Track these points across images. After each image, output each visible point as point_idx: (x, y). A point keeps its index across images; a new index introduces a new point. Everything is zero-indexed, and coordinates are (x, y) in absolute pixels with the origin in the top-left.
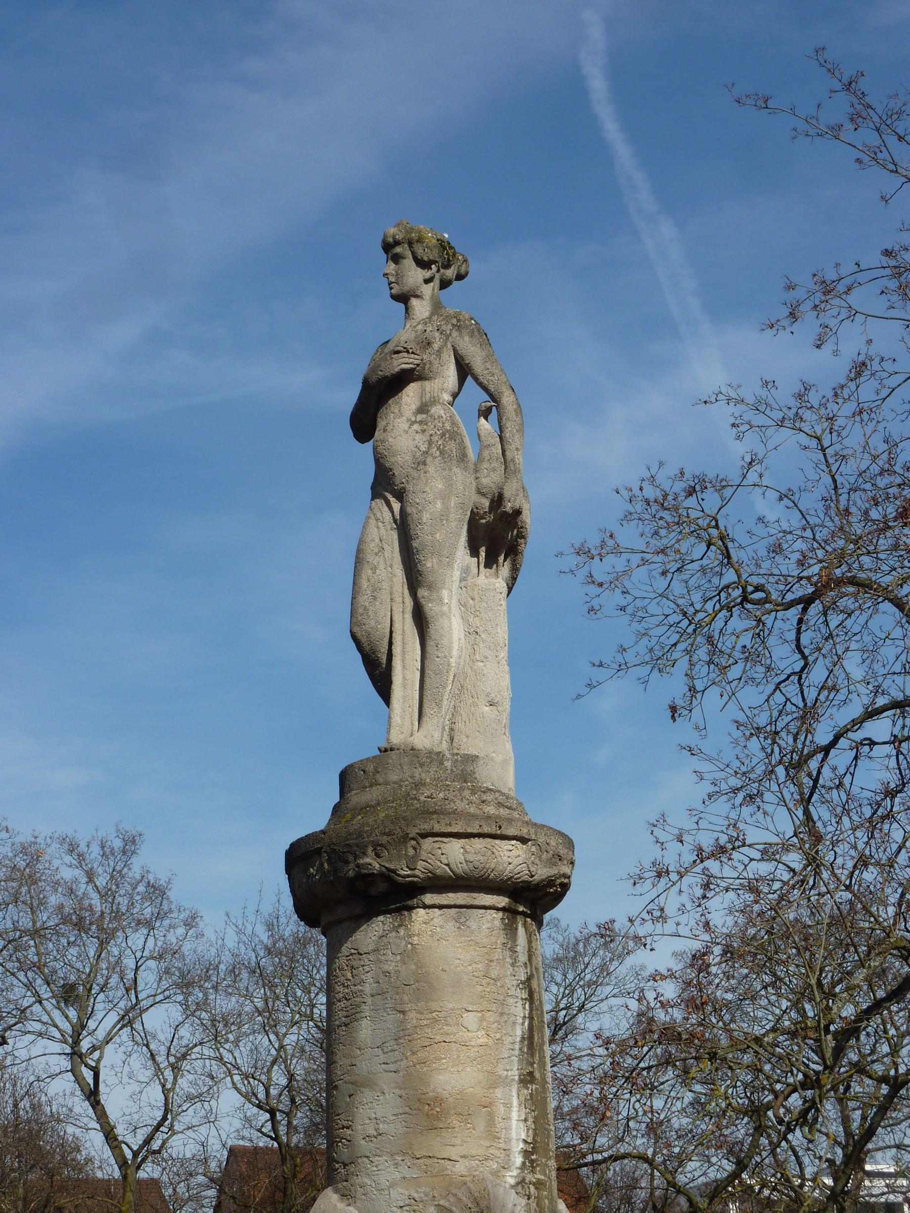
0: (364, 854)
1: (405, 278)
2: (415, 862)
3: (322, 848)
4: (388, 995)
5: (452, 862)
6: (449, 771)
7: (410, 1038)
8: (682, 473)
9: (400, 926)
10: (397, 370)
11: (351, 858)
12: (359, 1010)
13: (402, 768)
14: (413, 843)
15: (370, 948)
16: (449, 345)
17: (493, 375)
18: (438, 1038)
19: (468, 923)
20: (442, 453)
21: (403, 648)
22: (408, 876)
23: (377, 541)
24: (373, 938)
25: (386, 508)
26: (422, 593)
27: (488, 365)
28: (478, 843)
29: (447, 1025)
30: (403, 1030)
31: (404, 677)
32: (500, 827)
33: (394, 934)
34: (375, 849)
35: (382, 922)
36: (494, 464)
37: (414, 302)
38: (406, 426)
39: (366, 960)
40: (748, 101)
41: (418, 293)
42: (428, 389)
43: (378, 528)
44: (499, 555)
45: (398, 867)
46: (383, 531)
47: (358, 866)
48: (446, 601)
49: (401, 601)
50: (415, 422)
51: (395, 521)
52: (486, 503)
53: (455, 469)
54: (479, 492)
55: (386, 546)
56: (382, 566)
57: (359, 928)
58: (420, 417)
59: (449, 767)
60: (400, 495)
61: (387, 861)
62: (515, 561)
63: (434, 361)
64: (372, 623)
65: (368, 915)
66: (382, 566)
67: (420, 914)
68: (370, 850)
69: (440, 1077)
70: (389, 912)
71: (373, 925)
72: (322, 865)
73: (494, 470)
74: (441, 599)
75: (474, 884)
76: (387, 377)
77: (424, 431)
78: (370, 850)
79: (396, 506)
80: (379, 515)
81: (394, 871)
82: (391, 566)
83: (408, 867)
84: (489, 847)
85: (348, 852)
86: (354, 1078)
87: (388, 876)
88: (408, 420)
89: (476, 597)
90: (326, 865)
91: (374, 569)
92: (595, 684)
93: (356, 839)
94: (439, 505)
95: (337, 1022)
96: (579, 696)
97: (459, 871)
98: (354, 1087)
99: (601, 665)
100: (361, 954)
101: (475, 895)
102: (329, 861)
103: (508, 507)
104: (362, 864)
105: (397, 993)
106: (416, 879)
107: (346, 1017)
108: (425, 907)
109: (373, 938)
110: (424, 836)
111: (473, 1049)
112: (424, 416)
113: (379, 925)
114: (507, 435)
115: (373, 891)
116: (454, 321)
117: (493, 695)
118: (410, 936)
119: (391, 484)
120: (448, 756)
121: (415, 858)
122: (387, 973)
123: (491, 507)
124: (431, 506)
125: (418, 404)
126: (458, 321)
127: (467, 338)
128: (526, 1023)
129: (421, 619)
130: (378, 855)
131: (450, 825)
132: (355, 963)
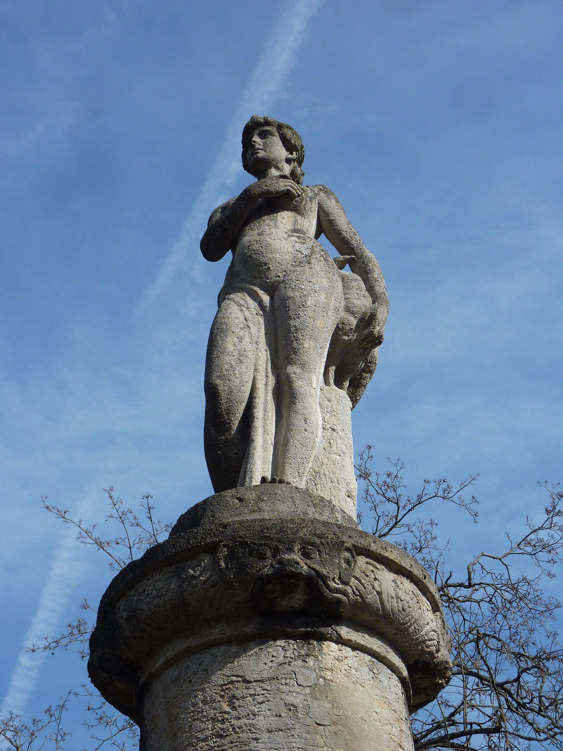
0: (290, 550)
3: (221, 541)
5: (384, 591)
9: (308, 655)
11: (269, 554)
13: (294, 501)
14: (347, 555)
16: (317, 202)
19: (380, 677)
21: (265, 415)
22: (338, 591)
23: (242, 319)
28: (409, 586)
31: (264, 441)
33: (300, 662)
35: (283, 648)
38: (286, 236)
39: (258, 689)
40: (53, 510)
42: (299, 221)
45: (331, 575)
46: (247, 314)
47: (281, 562)
48: (314, 386)
49: (264, 374)
50: (293, 236)
52: (353, 321)
54: (348, 310)
55: (251, 325)
56: (247, 339)
60: (272, 289)
61: (319, 564)
63: (308, 202)
64: (237, 382)
65: (263, 637)
66: (247, 339)
67: (331, 648)
68: (297, 547)
70: (294, 637)
71: (270, 650)
72: (216, 562)
78: (297, 547)
79: (266, 299)
80: (242, 302)
81: (324, 579)
83: (340, 578)
85: (266, 545)
87: (314, 583)
90: (222, 564)
91: (241, 339)
93: (276, 533)
101: (389, 649)
102: (231, 557)
104: (288, 560)
105: (308, 732)
106: (344, 598)
108: (340, 641)
113: (280, 650)
114: (376, 276)
115: (284, 604)
119: (261, 278)
122: (292, 708)
123: (358, 326)
130: (306, 555)
132: (238, 693)
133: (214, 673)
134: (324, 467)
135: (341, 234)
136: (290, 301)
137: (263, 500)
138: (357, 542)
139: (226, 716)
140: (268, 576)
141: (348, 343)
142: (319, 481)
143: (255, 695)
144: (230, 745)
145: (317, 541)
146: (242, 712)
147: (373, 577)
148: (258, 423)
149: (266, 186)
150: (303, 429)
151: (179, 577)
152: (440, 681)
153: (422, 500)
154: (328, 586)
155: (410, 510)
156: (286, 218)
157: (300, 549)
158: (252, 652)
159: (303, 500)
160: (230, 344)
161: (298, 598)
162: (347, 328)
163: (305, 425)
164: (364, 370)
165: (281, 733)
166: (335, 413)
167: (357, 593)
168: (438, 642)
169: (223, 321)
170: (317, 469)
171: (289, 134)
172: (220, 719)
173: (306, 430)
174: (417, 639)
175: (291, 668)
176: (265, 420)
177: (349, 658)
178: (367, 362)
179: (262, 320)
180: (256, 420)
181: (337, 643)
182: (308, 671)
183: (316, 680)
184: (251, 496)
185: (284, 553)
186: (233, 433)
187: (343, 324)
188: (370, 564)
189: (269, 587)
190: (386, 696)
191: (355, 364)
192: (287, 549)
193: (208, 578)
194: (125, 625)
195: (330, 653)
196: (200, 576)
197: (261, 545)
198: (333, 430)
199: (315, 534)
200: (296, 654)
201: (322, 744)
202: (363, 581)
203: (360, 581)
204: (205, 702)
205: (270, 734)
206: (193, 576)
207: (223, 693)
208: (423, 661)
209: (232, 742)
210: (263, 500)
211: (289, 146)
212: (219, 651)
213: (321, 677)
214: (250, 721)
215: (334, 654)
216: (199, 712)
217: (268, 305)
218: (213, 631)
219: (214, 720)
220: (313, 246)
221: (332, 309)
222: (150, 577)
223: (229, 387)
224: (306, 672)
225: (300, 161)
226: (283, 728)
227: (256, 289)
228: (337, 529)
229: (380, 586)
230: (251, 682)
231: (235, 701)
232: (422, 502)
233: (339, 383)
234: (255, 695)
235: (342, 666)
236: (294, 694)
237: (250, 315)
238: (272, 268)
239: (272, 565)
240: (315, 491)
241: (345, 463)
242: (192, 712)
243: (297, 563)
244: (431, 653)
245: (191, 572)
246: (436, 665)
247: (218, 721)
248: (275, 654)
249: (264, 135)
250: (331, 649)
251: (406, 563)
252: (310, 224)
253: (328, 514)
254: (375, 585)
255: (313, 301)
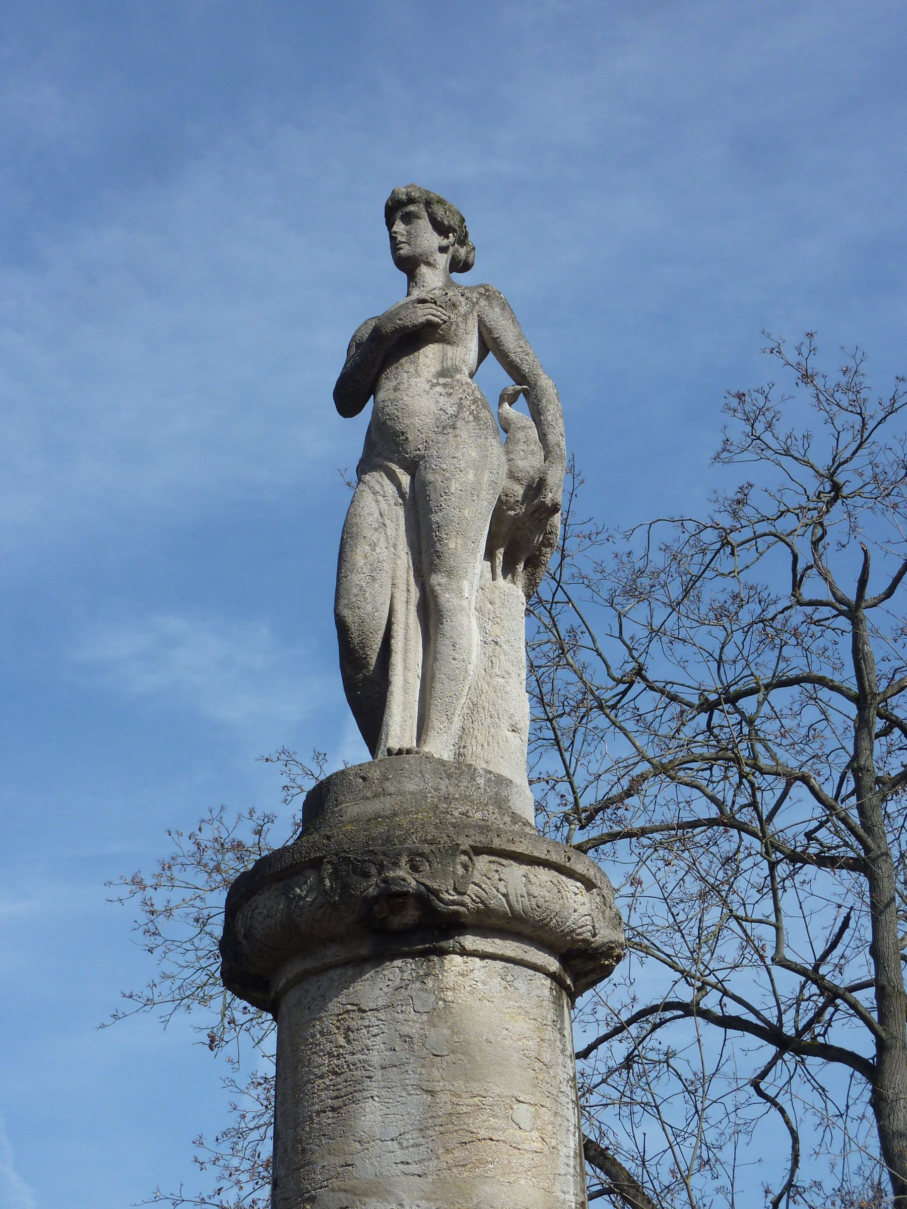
0: (396, 864)
1: (419, 239)
2: (466, 884)
3: (324, 857)
4: (409, 1068)
5: (512, 892)
6: (482, 791)
7: (442, 1129)
8: (251, 812)
9: (427, 975)
10: (421, 320)
11: (374, 870)
12: (358, 1087)
13: (423, 776)
14: (464, 858)
15: (381, 1002)
16: (475, 314)
17: (528, 354)
18: (483, 1133)
19: (516, 984)
20: (477, 418)
22: (453, 903)
23: (377, 514)
24: (386, 990)
25: (386, 482)
26: (437, 580)
27: (522, 343)
28: (544, 875)
29: (494, 1116)
30: (432, 1117)
32: (569, 859)
33: (418, 985)
34: (411, 860)
35: (400, 969)
36: (532, 447)
37: (424, 269)
38: (427, 387)
39: (373, 1019)
41: (431, 260)
42: (449, 354)
43: (377, 501)
44: (517, 563)
45: (443, 888)
46: (383, 505)
47: (385, 881)
49: (405, 588)
50: (438, 384)
51: (402, 494)
52: (519, 491)
53: (491, 439)
54: (512, 476)
55: (388, 522)
56: (383, 544)
57: (361, 975)
58: (442, 380)
59: (482, 786)
60: (413, 466)
61: (428, 877)
62: (533, 575)
63: (460, 324)
64: (369, 608)
66: (383, 544)
68: (404, 860)
69: (487, 1188)
70: (412, 955)
71: (386, 972)
72: (321, 881)
73: (533, 453)
74: (461, 591)
75: (527, 930)
76: (407, 327)
77: (451, 394)
78: (404, 860)
79: (405, 479)
80: (378, 488)
81: (436, 893)
82: (395, 546)
83: (455, 889)
84: (556, 882)
86: (354, 1183)
87: (425, 899)
88: (429, 381)
89: (497, 601)
90: (328, 883)
91: (373, 546)
92: (121, 1015)
93: (382, 845)
94: (471, 477)
95: (317, 1107)
96: (103, 1026)
97: (518, 907)
98: (349, 1196)
99: (131, 997)
100: (364, 1011)
101: (526, 947)
102: (335, 876)
103: (549, 498)
104: (393, 878)
105: (423, 1066)
106: (462, 909)
107: (337, 1097)
108: (464, 952)
109: (386, 990)
110: (478, 851)
111: (527, 1156)
112: (449, 380)
113: (397, 971)
114: (549, 418)
115: (396, 922)
116: (482, 290)
117: (517, 719)
118: (441, 990)
119: (399, 452)
120: (482, 772)
121: (466, 878)
122: (407, 1039)
123: (525, 496)
124: (462, 475)
125: (439, 368)
126: (487, 290)
127: (497, 310)
128: (577, 1135)
129: (430, 613)
130: (415, 868)
131: (513, 841)
132: (353, 1024)
133: (331, 1000)
134: (483, 697)
135: (508, 357)
136: (430, 487)
137: (388, 779)
138: (475, 841)
139: (341, 1051)
140: (373, 898)
141: (516, 518)
142: (476, 716)
143: (369, 1026)
144: (344, 1084)
145: (426, 848)
146: (357, 1046)
147: (497, 877)
148: (397, 660)
149: (400, 319)
150: (451, 657)
151: (288, 897)
152: (607, 962)
153: (896, 406)
154: (441, 900)
155: (879, 423)
156: (431, 356)
157: (407, 862)
158: (368, 976)
159: (435, 772)
160: (360, 557)
161: (411, 915)
162: (512, 500)
163: (453, 653)
164: (543, 544)
165: (395, 1069)
166: (499, 620)
167: (478, 900)
168: (593, 927)
169: (354, 521)
170: (475, 700)
171: (439, 211)
172: (335, 1053)
173: (454, 659)
174: (563, 931)
175: (408, 992)
176: (406, 651)
177: (475, 971)
178: (546, 534)
179: (401, 512)
180: (393, 654)
181: (462, 955)
182: (426, 995)
183: (435, 1004)
184: (375, 774)
185: (389, 869)
186: (372, 669)
187: (506, 495)
188: (494, 862)
189: (377, 907)
190: (522, 1005)
191: (529, 541)
192: (393, 863)
193: (314, 900)
194: (244, 942)
195: (453, 969)
196: (306, 896)
197: (365, 861)
198: (496, 643)
199: (426, 841)
200: (414, 975)
201: (439, 1077)
202: (483, 886)
203: (480, 887)
204: (322, 1033)
205: (383, 1071)
206: (300, 895)
207: (338, 1024)
208: (578, 949)
209: (346, 1081)
210: (388, 779)
211: (441, 229)
212: (336, 974)
213: (440, 999)
214: (364, 1057)
215: (458, 969)
216: (317, 1045)
217: (408, 490)
218: (328, 953)
219: (330, 1055)
220: (461, 399)
221: (485, 486)
222: (260, 892)
223: (360, 617)
224: (424, 995)
225: (462, 240)
226: (397, 1064)
227: (395, 467)
228: (452, 829)
229: (506, 887)
230: (366, 1011)
231: (350, 1033)
232: (896, 410)
233: (509, 569)
234: (369, 1026)
235: (468, 982)
236: (410, 1023)
237: (386, 507)
238: (410, 438)
239: (377, 885)
240: (471, 730)
241: (508, 689)
242: (311, 1043)
243: (404, 880)
244: (585, 941)
245: (298, 890)
246: (596, 949)
247: (334, 1056)
248: (391, 977)
249: (408, 218)
250: (454, 963)
251: (540, 852)
252: (468, 349)
253: (465, 784)
254: (500, 887)
255: (457, 485)
